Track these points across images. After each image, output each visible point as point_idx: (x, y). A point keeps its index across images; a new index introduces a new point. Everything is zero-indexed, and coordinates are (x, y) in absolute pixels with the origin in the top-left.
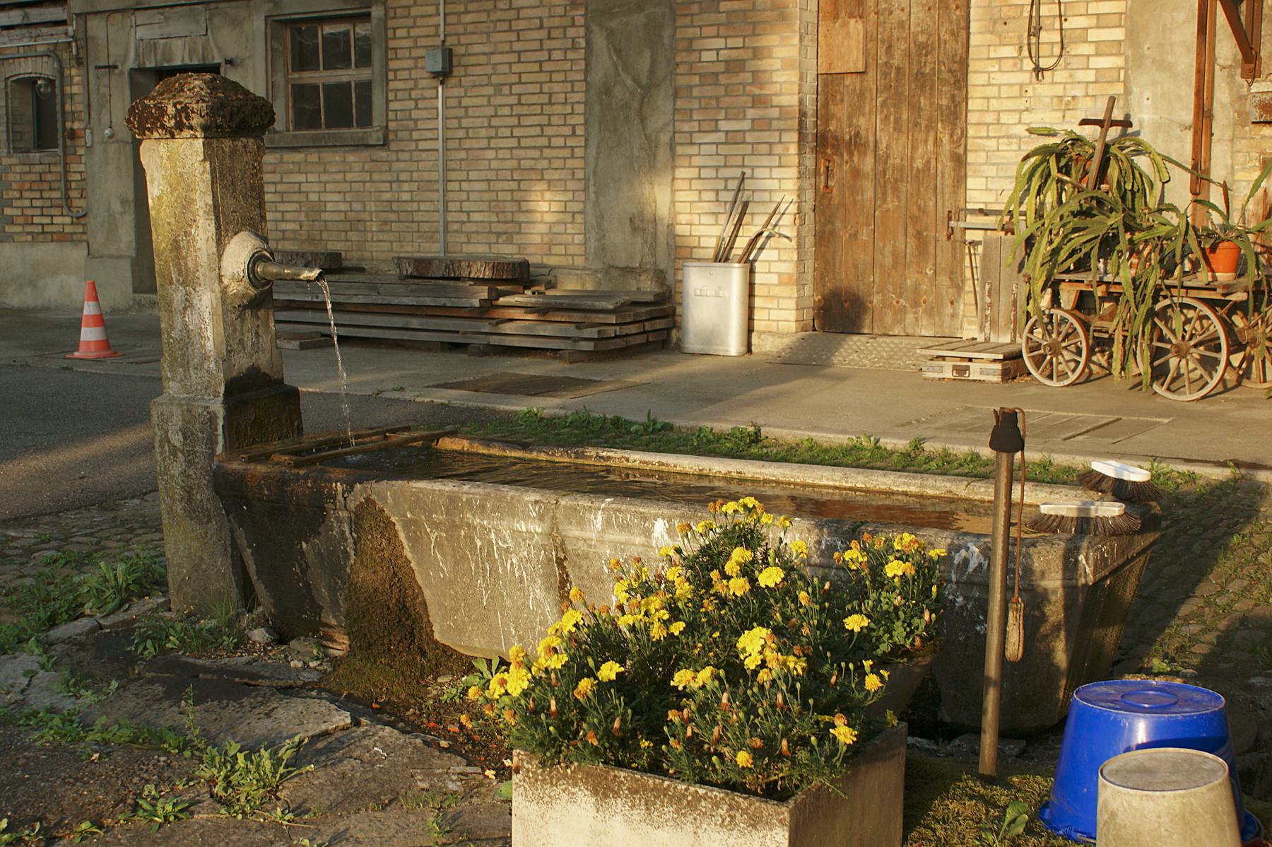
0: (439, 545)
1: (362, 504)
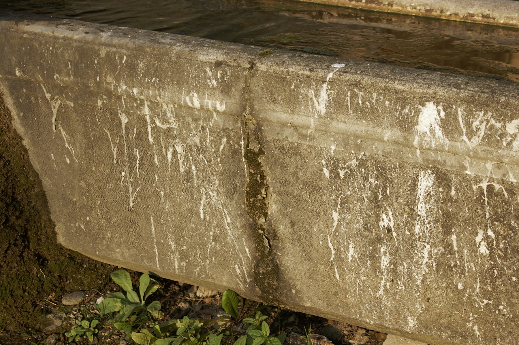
0: (63, 117)
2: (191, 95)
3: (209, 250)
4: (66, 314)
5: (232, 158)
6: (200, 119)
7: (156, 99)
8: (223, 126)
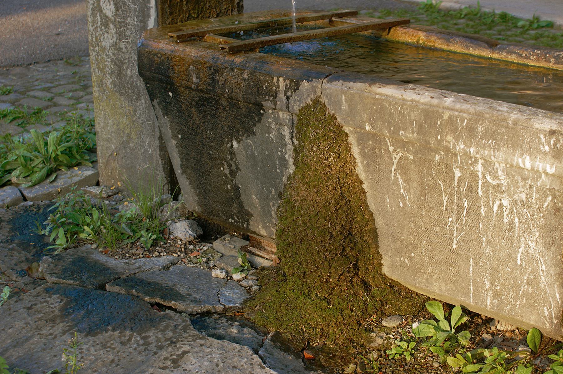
0: (403, 168)
1: (307, 107)
2: (524, 157)
3: (521, 292)
4: (387, 334)
5: (555, 214)
6: (528, 179)
7: (490, 159)
8: (550, 186)
